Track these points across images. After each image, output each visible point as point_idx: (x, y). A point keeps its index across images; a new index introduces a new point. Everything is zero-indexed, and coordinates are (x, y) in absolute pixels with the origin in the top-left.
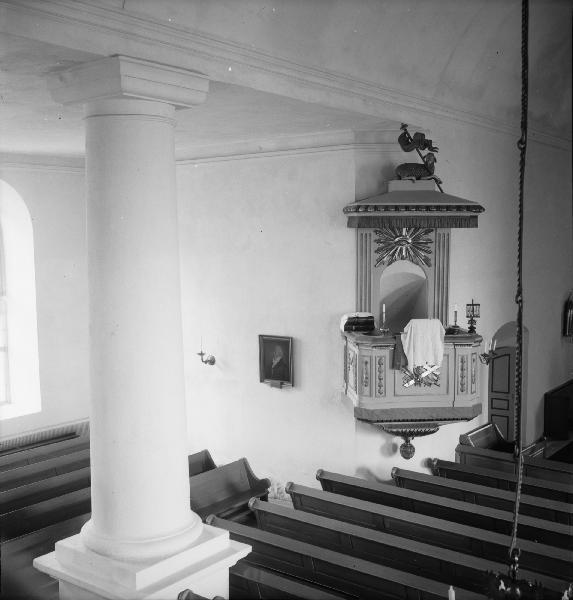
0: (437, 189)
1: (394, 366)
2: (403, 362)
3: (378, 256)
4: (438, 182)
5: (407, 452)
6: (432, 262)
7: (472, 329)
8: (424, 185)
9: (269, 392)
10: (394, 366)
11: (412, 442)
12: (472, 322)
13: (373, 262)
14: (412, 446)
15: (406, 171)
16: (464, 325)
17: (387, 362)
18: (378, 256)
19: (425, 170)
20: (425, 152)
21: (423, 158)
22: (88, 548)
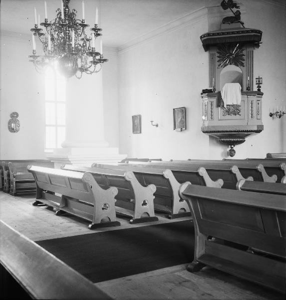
0: (242, 27)
1: (218, 106)
2: (222, 104)
3: (219, 63)
4: (243, 24)
5: (232, 153)
6: (245, 65)
7: (259, 90)
8: (234, 26)
9: (177, 134)
10: (218, 106)
11: (234, 148)
12: (259, 87)
13: (217, 66)
14: (234, 151)
15: (227, 20)
16: (255, 89)
17: (215, 104)
18: (219, 63)
19: (237, 18)
20: (235, 10)
21: (234, 14)
22: (62, 147)
